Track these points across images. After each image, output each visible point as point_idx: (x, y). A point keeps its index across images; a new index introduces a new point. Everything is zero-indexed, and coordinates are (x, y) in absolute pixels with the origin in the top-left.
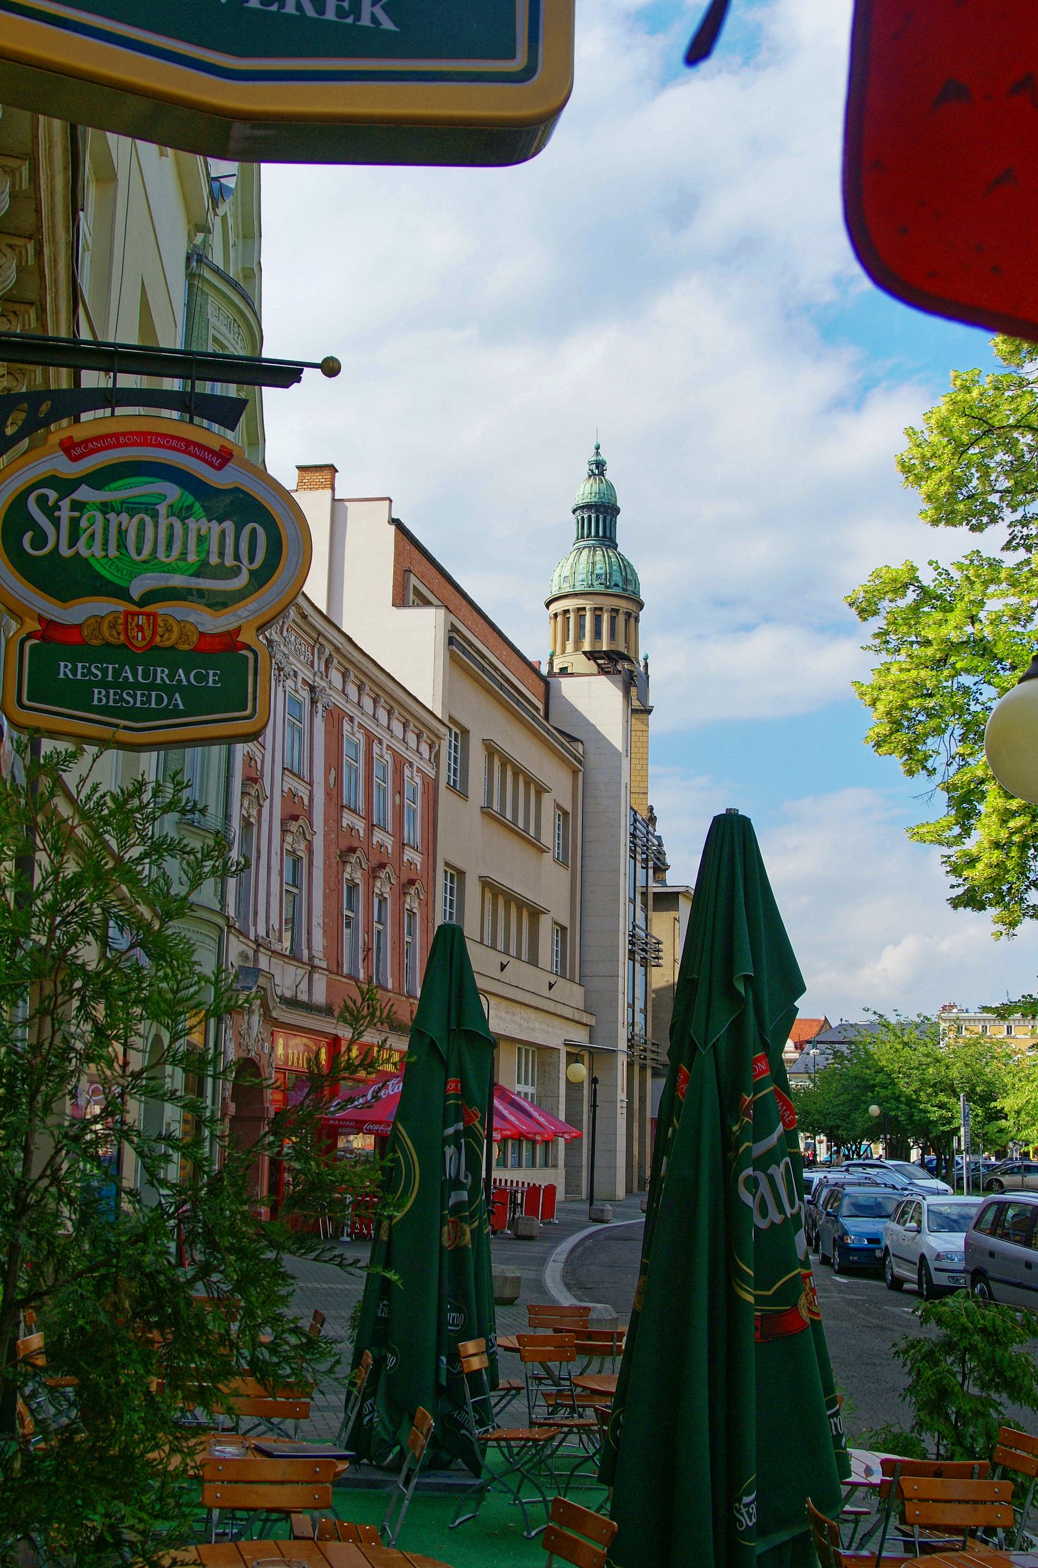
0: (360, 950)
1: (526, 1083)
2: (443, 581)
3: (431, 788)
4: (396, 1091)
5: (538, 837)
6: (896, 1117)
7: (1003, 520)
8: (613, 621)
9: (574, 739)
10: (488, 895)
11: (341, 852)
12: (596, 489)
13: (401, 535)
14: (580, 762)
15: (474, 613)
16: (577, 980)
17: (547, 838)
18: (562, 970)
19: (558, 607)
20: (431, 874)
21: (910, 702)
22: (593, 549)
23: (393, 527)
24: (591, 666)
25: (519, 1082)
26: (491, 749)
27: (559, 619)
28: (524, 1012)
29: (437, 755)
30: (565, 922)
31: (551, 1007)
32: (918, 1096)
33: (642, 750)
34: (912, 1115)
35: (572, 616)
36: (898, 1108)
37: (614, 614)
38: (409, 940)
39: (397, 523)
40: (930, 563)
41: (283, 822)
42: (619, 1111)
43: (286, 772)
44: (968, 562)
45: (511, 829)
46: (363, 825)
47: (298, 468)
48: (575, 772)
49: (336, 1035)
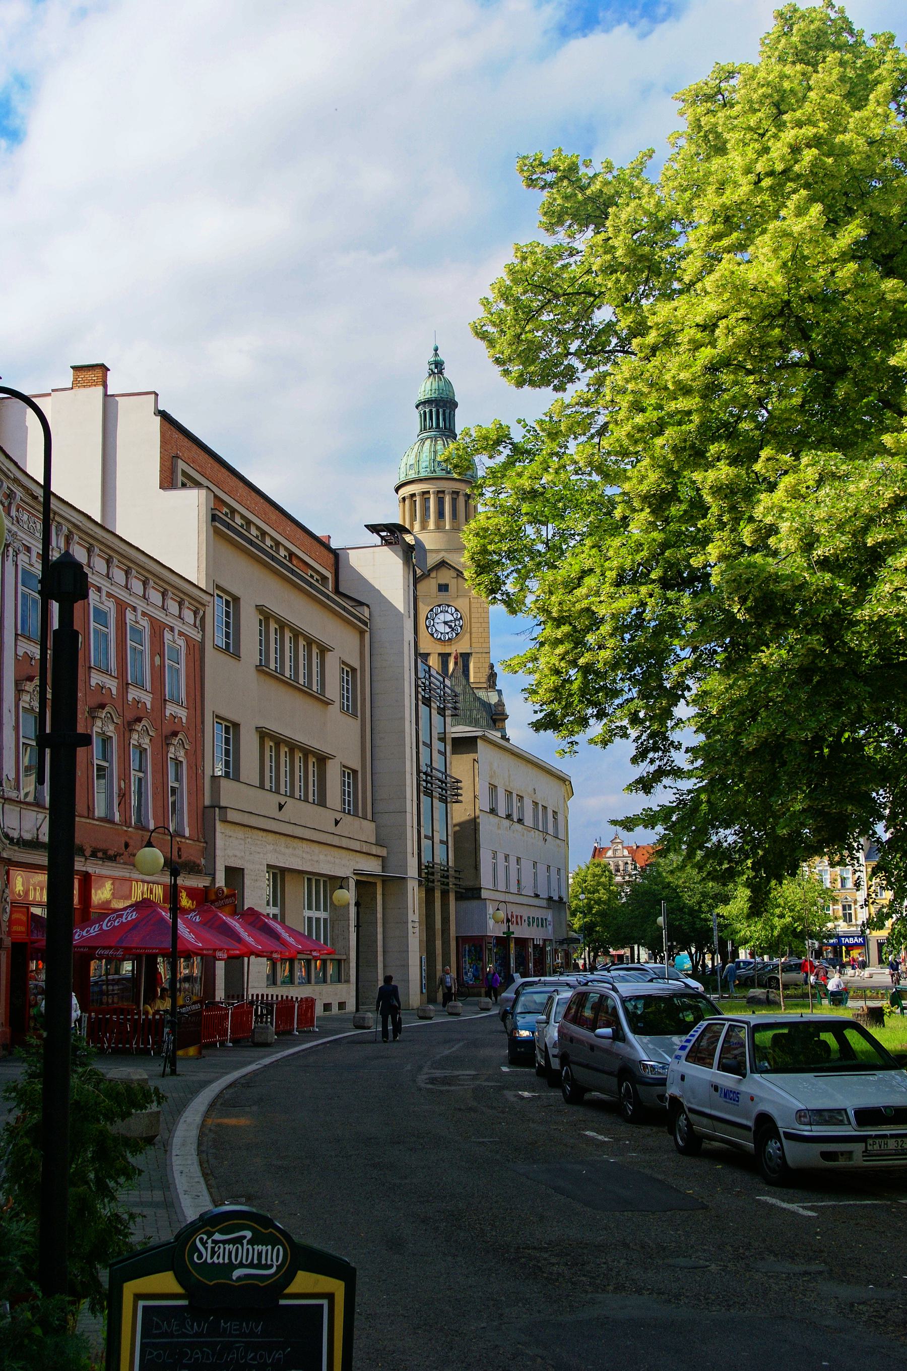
0: (115, 796)
1: (318, 909)
2: (217, 466)
3: (197, 652)
4: (129, 919)
5: (323, 692)
6: (680, 925)
7: (579, 379)
8: (454, 502)
9: (361, 604)
10: (269, 743)
11: (90, 708)
12: (435, 386)
13: (168, 425)
14: (366, 624)
15: (253, 494)
16: (369, 816)
17: (333, 690)
18: (352, 808)
19: (406, 491)
20: (199, 727)
21: (489, 547)
22: (434, 439)
23: (159, 418)
24: (376, 539)
25: (310, 908)
26: (266, 615)
27: (407, 502)
28: (305, 845)
29: (203, 619)
30: (356, 764)
31: (336, 841)
32: (700, 907)
33: (483, 615)
34: (695, 924)
35: (418, 499)
36: (682, 918)
37: (455, 496)
38: (176, 785)
39: (164, 416)
40: (519, 421)
41: (17, 683)
42: (410, 930)
43: (20, 638)
44: (547, 419)
45: (291, 685)
46: (116, 684)
47: (72, 367)
48: (362, 633)
49: (87, 873)
